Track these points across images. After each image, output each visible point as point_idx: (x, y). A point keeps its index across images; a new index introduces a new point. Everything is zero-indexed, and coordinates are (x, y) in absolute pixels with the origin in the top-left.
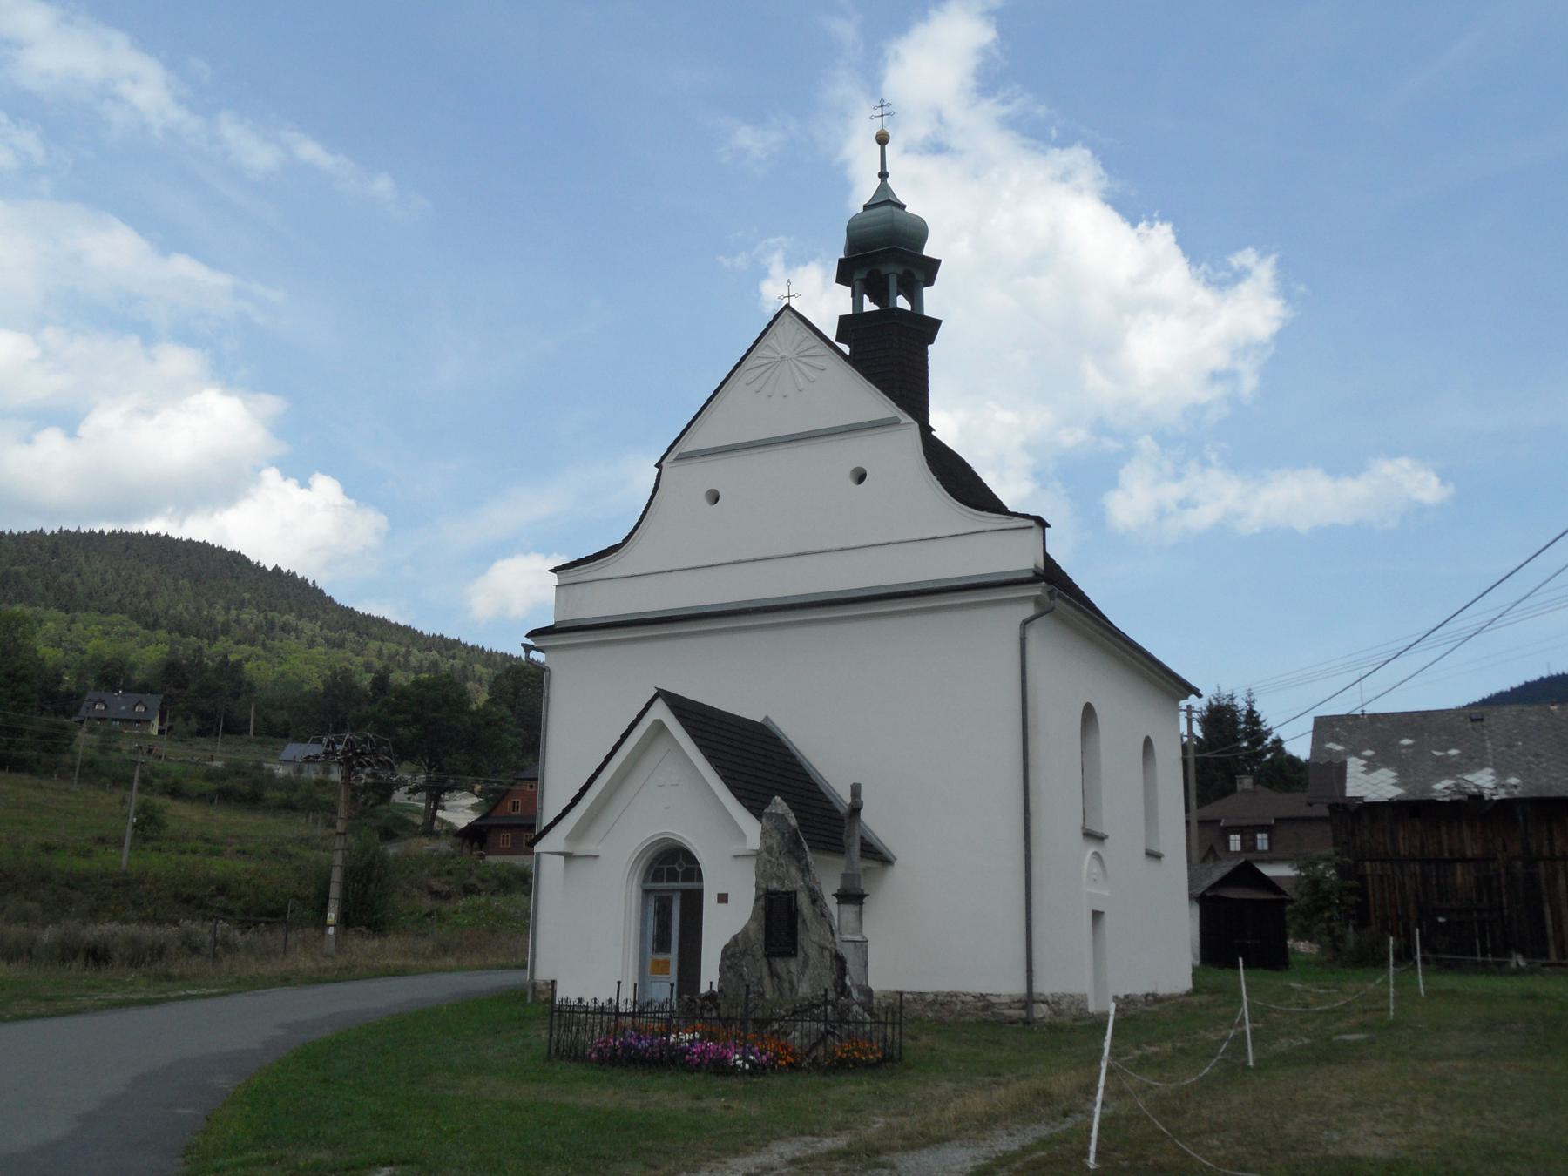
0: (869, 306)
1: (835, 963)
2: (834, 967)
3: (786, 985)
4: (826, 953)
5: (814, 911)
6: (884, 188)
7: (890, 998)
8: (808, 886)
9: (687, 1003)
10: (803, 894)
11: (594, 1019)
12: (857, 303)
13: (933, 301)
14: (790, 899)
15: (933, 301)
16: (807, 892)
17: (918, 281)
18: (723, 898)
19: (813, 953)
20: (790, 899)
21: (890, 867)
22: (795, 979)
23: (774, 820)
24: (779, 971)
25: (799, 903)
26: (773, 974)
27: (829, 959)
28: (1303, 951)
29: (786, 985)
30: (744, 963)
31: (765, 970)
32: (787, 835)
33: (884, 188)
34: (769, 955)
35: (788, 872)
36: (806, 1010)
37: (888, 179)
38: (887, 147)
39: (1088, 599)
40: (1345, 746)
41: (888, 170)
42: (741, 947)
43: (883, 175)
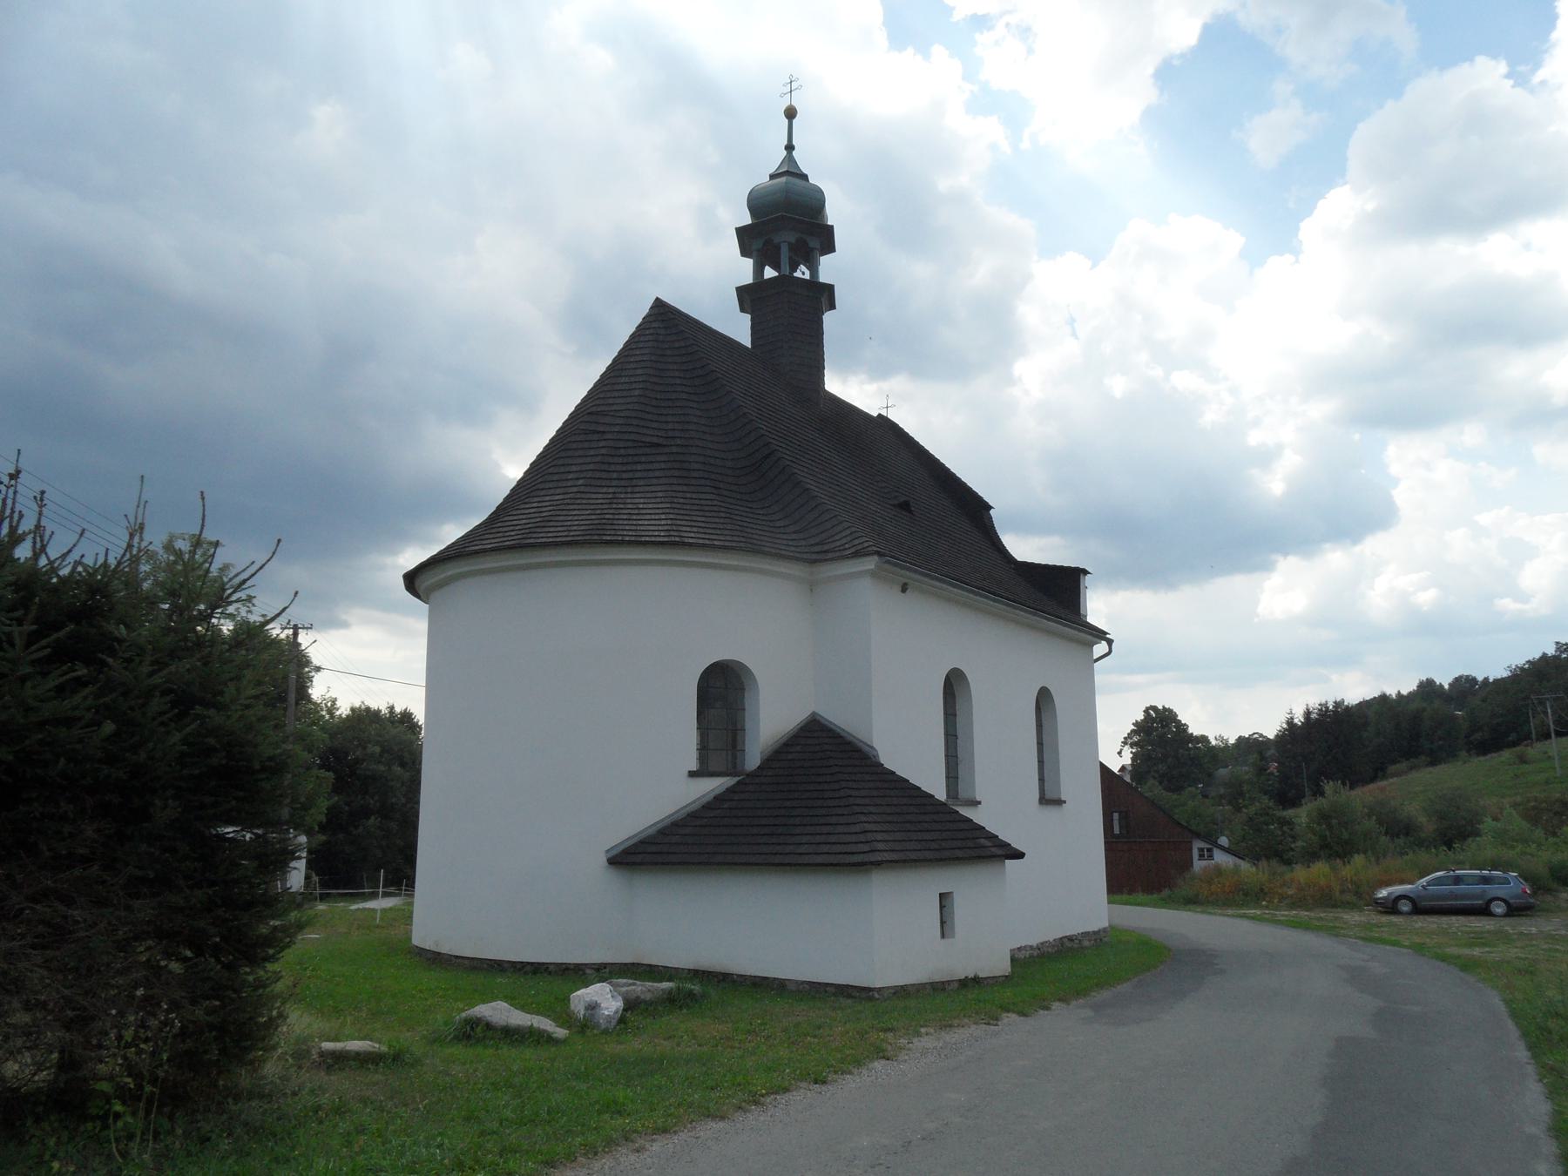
0: (769, 273)
6: (789, 159)
9: (595, 1147)
12: (758, 271)
13: (829, 269)
15: (829, 269)
17: (812, 250)
28: (269, 931)
33: (789, 159)
37: (794, 153)
38: (795, 121)
41: (794, 143)
43: (790, 148)
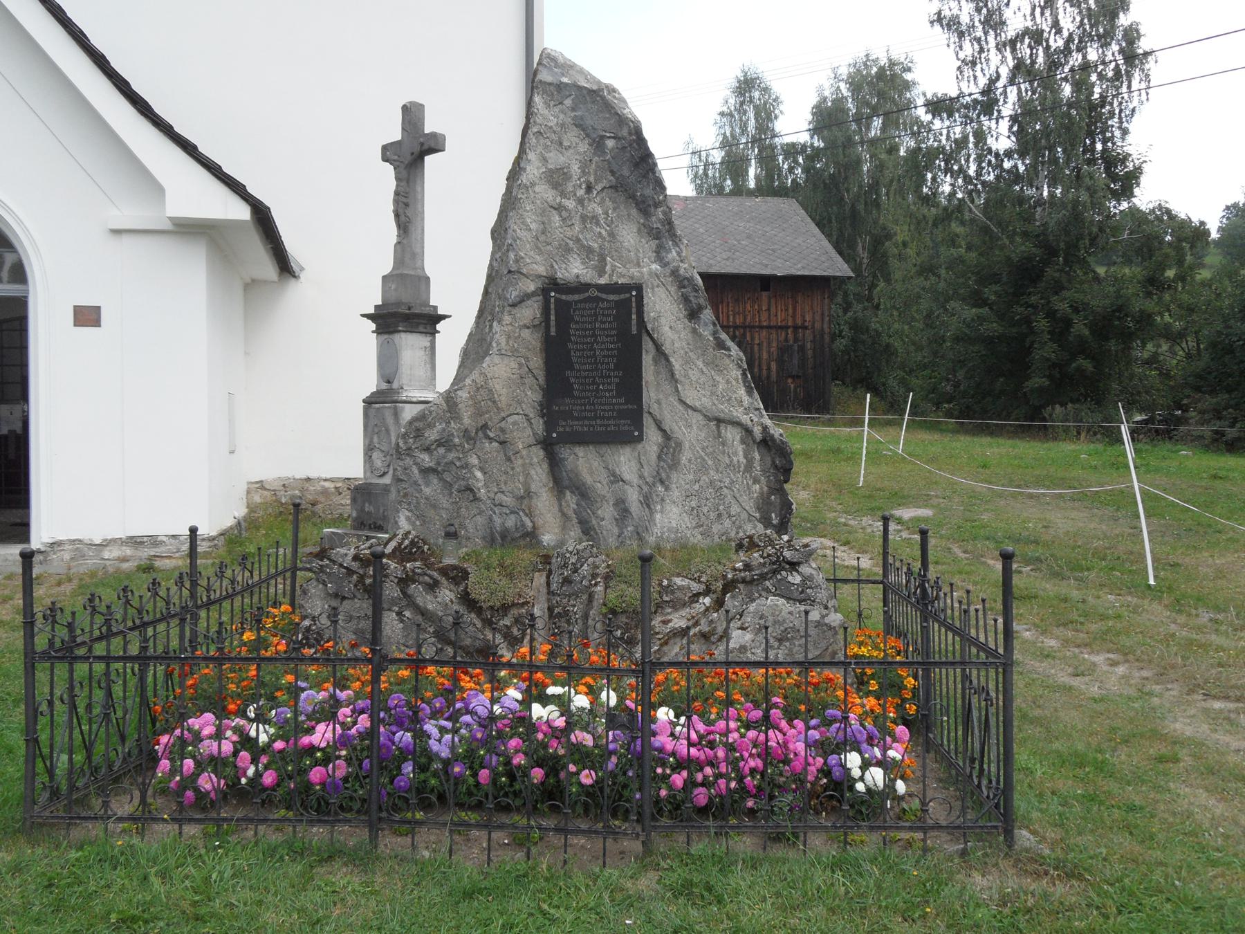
1: (757, 456)
2: (757, 465)
3: (607, 512)
4: (732, 435)
5: (694, 331)
7: (294, 489)
8: (675, 273)
10: (661, 292)
11: (125, 658)
14: (623, 306)
16: (673, 289)
18: (87, 317)
19: (691, 434)
20: (623, 306)
21: (293, 280)
22: (633, 496)
23: (568, 102)
24: (587, 478)
25: (650, 314)
26: (561, 481)
27: (740, 449)
29: (607, 512)
30: (474, 460)
31: (539, 475)
32: (610, 143)
34: (548, 446)
35: (612, 234)
36: (763, 577)
39: (108, 62)
40: (806, 181)
42: (467, 421)
